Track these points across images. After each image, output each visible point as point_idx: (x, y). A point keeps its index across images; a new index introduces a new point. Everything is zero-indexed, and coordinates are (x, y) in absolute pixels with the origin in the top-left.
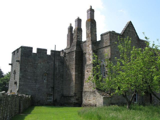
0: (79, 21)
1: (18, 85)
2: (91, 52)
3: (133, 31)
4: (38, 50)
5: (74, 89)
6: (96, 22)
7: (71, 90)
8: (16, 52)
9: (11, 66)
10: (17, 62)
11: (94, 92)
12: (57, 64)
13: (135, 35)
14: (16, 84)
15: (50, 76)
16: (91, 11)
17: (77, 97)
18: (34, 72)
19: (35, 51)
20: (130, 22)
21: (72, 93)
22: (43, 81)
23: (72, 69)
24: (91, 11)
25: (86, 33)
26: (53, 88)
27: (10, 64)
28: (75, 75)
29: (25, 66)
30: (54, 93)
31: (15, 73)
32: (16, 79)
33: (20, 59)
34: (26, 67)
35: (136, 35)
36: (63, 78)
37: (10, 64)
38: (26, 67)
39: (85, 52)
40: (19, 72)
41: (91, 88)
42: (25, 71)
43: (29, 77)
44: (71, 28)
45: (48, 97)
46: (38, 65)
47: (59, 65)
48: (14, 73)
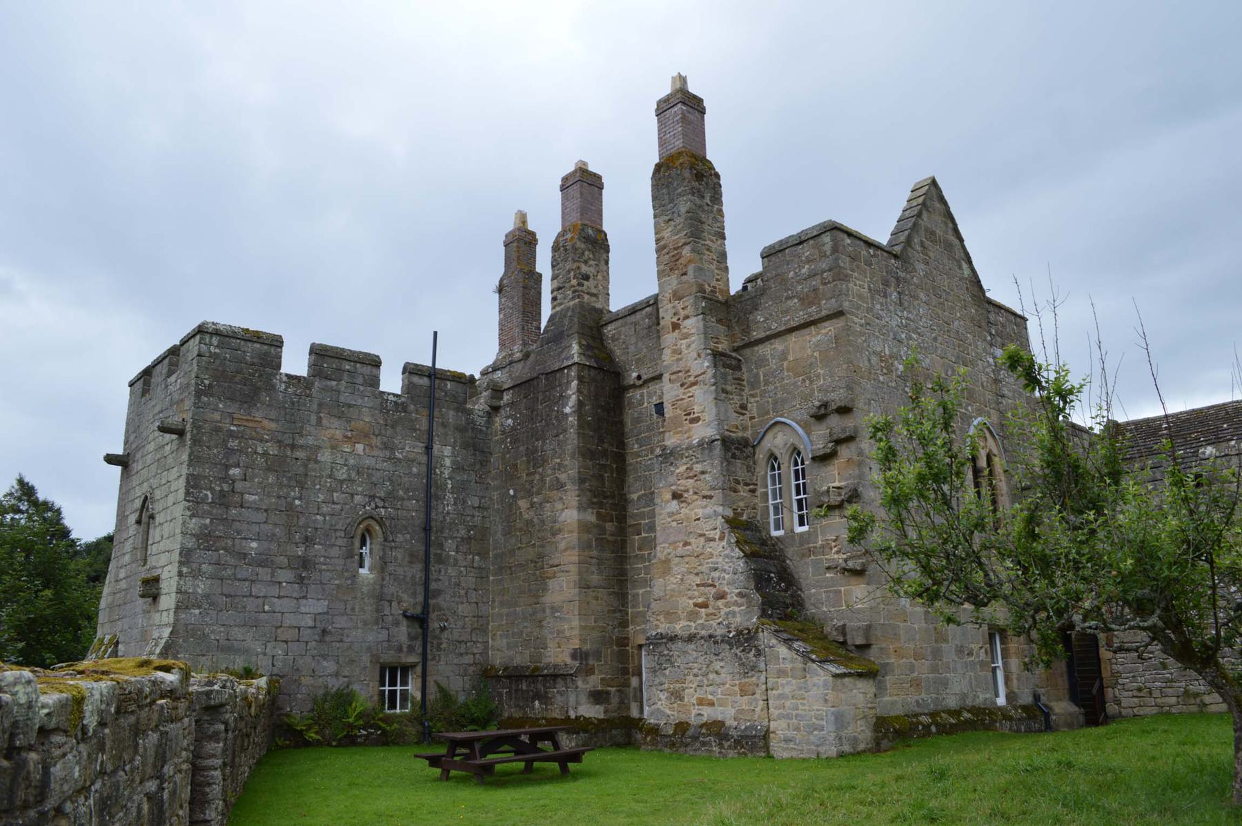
0: (584, 186)
1: (168, 601)
2: (702, 366)
3: (957, 242)
4: (320, 354)
5: (576, 623)
6: (717, 176)
7: (546, 632)
8: (163, 368)
9: (117, 470)
10: (168, 437)
11: (745, 639)
12: (446, 454)
13: (960, 267)
14: (155, 598)
15: (400, 538)
16: (683, 108)
17: (594, 682)
18: (290, 508)
19: (295, 363)
20: (934, 182)
21: (558, 655)
22: (355, 576)
23: (560, 486)
24: (683, 108)
25: (654, 246)
26: (420, 620)
27: (110, 459)
28: (584, 527)
29: (227, 467)
30: (424, 655)
31: (152, 517)
32: (152, 561)
33: (188, 416)
34: (234, 471)
35: (965, 266)
36: (483, 554)
37: (110, 459)
38: (231, 472)
39: (639, 377)
40: (179, 511)
41: (710, 610)
42: (223, 500)
43: (254, 545)
44: (521, 243)
45: (387, 688)
46: (316, 462)
47: (458, 468)
48: (139, 522)
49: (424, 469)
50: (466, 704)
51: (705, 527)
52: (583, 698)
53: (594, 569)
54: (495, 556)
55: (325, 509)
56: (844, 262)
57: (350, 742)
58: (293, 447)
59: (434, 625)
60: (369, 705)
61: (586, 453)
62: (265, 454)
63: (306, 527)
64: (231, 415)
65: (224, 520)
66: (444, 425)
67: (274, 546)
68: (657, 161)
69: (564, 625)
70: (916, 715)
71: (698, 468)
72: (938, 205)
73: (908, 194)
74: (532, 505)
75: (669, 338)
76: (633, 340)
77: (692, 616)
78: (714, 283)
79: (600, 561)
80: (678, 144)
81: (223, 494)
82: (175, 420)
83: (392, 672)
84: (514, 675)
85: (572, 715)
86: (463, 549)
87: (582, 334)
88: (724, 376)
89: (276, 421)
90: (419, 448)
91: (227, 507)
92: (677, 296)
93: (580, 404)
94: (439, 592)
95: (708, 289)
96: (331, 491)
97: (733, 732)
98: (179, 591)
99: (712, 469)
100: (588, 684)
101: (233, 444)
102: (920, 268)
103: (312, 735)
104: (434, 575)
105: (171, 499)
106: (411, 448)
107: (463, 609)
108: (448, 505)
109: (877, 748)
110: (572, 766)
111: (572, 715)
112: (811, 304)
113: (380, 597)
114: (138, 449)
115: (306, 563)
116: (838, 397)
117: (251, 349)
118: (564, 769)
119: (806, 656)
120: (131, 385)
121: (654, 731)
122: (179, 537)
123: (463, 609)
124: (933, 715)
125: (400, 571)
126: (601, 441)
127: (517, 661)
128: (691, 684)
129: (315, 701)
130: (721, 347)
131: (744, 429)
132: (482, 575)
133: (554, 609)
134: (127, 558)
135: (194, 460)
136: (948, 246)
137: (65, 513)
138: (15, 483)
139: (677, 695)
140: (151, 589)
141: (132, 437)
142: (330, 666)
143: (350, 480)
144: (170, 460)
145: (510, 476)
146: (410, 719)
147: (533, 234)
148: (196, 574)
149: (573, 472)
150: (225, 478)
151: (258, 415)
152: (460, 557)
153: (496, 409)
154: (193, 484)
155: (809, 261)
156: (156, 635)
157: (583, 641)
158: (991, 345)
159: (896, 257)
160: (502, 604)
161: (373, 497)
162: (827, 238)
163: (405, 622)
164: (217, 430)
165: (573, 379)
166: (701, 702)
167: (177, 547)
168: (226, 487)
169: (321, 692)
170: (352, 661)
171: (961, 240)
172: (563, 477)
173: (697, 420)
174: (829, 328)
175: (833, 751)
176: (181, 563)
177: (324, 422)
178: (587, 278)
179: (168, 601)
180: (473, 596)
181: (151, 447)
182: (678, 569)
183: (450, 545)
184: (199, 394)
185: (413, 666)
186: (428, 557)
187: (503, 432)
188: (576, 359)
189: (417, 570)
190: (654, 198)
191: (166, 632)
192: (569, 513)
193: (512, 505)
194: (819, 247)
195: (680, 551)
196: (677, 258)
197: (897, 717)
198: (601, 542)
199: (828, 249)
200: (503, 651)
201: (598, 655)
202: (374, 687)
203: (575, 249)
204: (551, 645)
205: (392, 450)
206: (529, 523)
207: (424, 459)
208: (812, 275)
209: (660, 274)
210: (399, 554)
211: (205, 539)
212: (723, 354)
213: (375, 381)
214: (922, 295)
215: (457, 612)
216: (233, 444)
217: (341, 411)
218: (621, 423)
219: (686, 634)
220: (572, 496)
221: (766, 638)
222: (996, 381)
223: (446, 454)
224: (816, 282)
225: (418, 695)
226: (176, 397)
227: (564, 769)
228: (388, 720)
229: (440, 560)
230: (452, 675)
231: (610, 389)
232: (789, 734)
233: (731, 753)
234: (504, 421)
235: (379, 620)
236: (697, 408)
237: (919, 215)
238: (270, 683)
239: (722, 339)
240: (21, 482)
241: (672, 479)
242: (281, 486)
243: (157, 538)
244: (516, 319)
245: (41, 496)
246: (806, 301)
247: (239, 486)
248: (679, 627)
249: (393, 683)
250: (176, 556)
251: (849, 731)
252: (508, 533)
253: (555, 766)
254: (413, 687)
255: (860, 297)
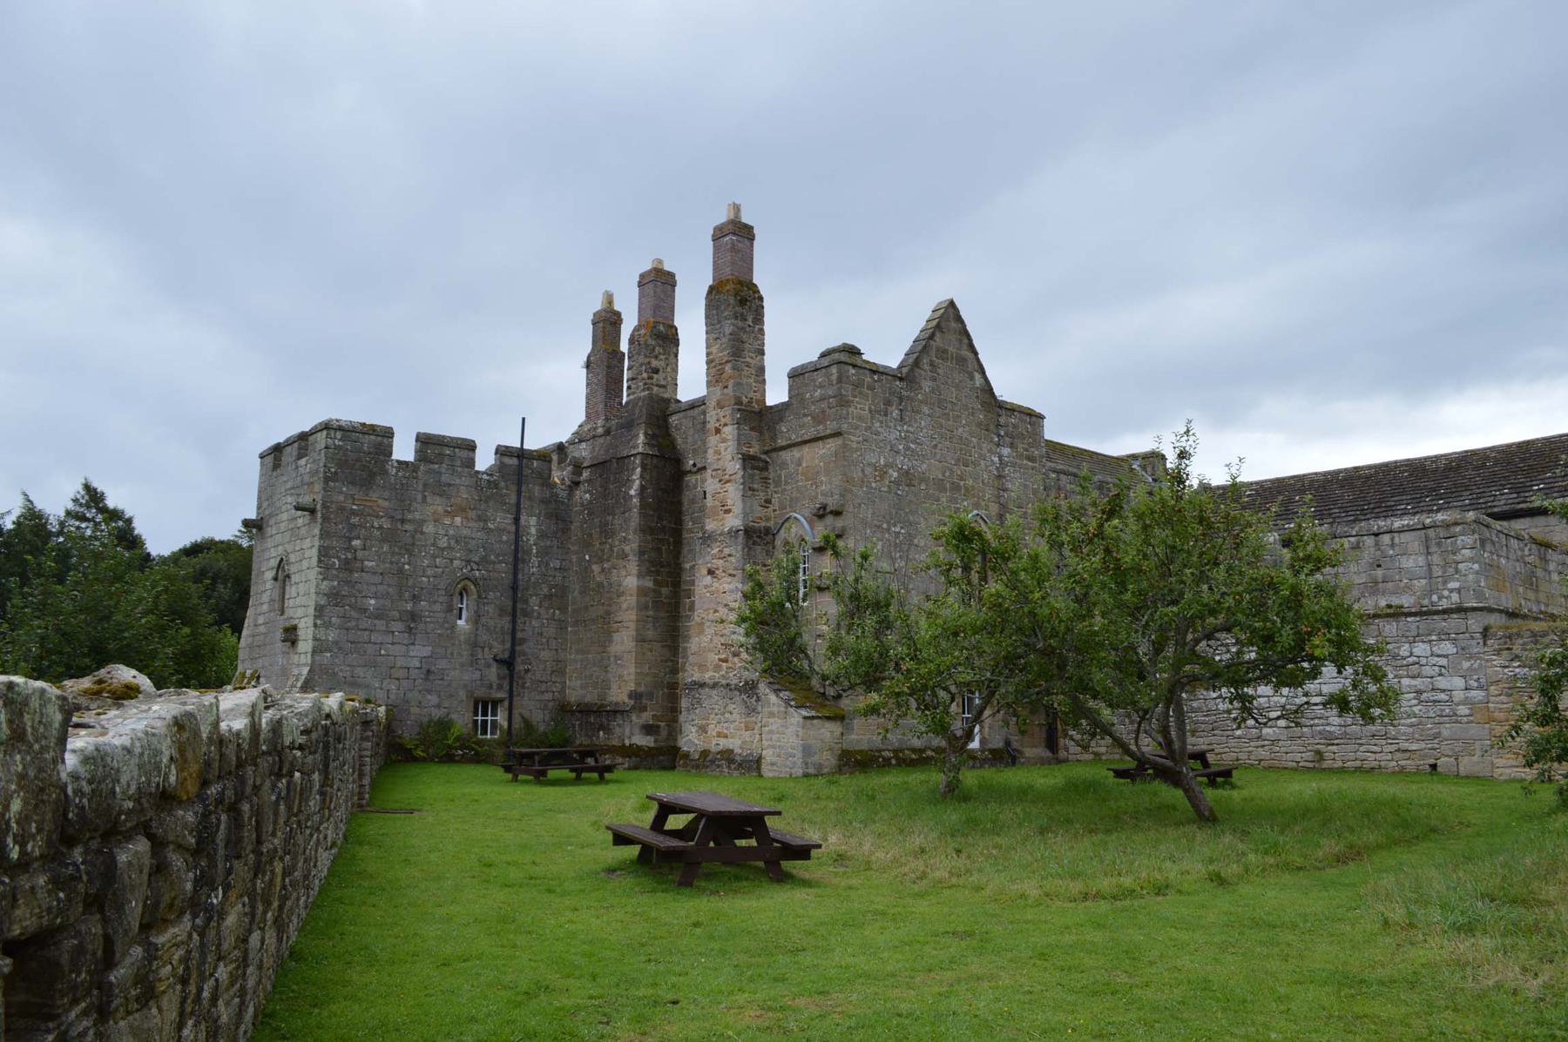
1: (305, 646)
2: (734, 467)
3: (971, 356)
4: (426, 442)
5: (632, 670)
11: (750, 688)
12: (531, 524)
13: (972, 378)
14: (294, 643)
17: (647, 717)
18: (401, 571)
20: (952, 304)
21: (619, 695)
22: (454, 626)
23: (624, 556)
24: (735, 238)
25: (704, 359)
26: (508, 663)
28: (642, 592)
29: (350, 539)
31: (288, 576)
32: (289, 612)
33: (319, 498)
34: (356, 543)
35: (977, 376)
36: (563, 609)
40: (313, 575)
42: (347, 566)
43: (372, 602)
44: (607, 322)
46: (422, 533)
47: (542, 535)
48: (276, 579)
49: (513, 537)
50: (545, 733)
51: (729, 598)
52: (637, 730)
53: (650, 626)
54: (574, 611)
55: (429, 572)
56: (847, 390)
57: (449, 759)
58: (403, 521)
59: (520, 667)
60: (465, 731)
61: (646, 530)
62: (381, 527)
63: (414, 587)
64: (352, 496)
65: (348, 582)
66: (529, 498)
67: (388, 603)
68: (711, 282)
69: (624, 672)
70: (879, 751)
71: (727, 551)
72: (953, 325)
73: (928, 314)
74: (603, 570)
75: (713, 440)
76: (691, 432)
77: (717, 668)
78: (752, 394)
79: (656, 619)
80: (727, 272)
81: (347, 561)
82: (306, 500)
83: (484, 705)
84: (585, 710)
85: (627, 742)
86: (546, 604)
87: (648, 424)
88: (752, 476)
89: (388, 500)
90: (509, 518)
91: (351, 571)
92: (720, 405)
93: (643, 488)
94: (523, 640)
95: (745, 400)
96: (434, 557)
97: (738, 758)
98: (315, 639)
99: (735, 551)
100: (639, 719)
101: (355, 520)
102: (927, 385)
103: (419, 753)
104: (520, 626)
105: (305, 564)
106: (502, 519)
107: (545, 655)
108: (533, 567)
109: (840, 770)
110: (607, 775)
111: (627, 742)
112: (820, 423)
113: (475, 645)
114: (271, 516)
115: (413, 617)
116: (832, 503)
117: (367, 442)
118: (602, 778)
119: (787, 702)
120: (262, 457)
121: (686, 756)
122: (313, 596)
123: (545, 655)
124: (896, 751)
125: (491, 623)
126: (660, 519)
127: (588, 699)
128: (713, 720)
129: (421, 726)
130: (752, 451)
131: (768, 519)
132: (562, 626)
133: (617, 658)
134: (265, 607)
135: (324, 534)
136: (961, 361)
137: (136, 524)
138: (80, 488)
139: (703, 729)
140: (291, 635)
141: (265, 505)
142: (433, 699)
143: (450, 548)
144: (303, 531)
145: (586, 545)
146: (499, 743)
147: (618, 314)
148: (328, 625)
149: (635, 546)
150: (349, 548)
151: (374, 495)
152: (542, 611)
153: (577, 484)
154: (324, 553)
155: (821, 387)
156: (296, 672)
157: (638, 684)
158: (998, 445)
159: (901, 379)
160: (577, 652)
161: (469, 562)
162: (834, 370)
163: (495, 665)
164: (342, 509)
165: (640, 458)
166: (719, 735)
167: (312, 604)
168: (349, 556)
169: (426, 720)
170: (451, 696)
171: (976, 354)
172: (627, 549)
173: (728, 511)
174: (832, 444)
175: (800, 772)
176: (316, 617)
177: (429, 499)
178: (656, 371)
179: (305, 646)
180: (553, 644)
181: (285, 516)
182: (710, 630)
183: (534, 600)
184: (327, 480)
185: (502, 700)
186: (515, 610)
187: (582, 505)
188: (640, 449)
189: (505, 622)
190: (707, 317)
191: (305, 671)
192: (630, 579)
193: (586, 570)
194: (828, 376)
195: (711, 617)
196: (721, 372)
197: (861, 751)
198: (657, 604)
199: (834, 377)
200: (576, 691)
201: (651, 696)
202: (469, 717)
203: (647, 345)
204: (614, 687)
205: (485, 521)
206: (600, 585)
207: (513, 528)
208: (822, 399)
209: (709, 384)
210: (490, 609)
211: (334, 597)
212: (753, 458)
213: (471, 463)
214: (926, 410)
215: (538, 656)
216: (355, 520)
217: (442, 490)
218: (680, 503)
219: (711, 682)
220: (633, 566)
221: (763, 688)
222: (1000, 477)
223: (531, 524)
224: (824, 405)
225: (505, 724)
226: (306, 479)
227: (602, 778)
228: (480, 743)
229: (526, 614)
230: (533, 708)
231: (670, 475)
232: (775, 759)
233: (736, 773)
234: (583, 495)
235: (474, 662)
236: (729, 502)
237: (932, 337)
238: (387, 711)
239: (754, 443)
240: (88, 487)
241: (708, 558)
242: (393, 554)
243: (294, 594)
244: (601, 396)
245: (111, 503)
246: (819, 419)
247: (360, 554)
248: (708, 676)
249: (485, 714)
250: (311, 611)
251: (816, 759)
252: (583, 592)
253: (595, 775)
254: (502, 718)
255: (860, 418)
